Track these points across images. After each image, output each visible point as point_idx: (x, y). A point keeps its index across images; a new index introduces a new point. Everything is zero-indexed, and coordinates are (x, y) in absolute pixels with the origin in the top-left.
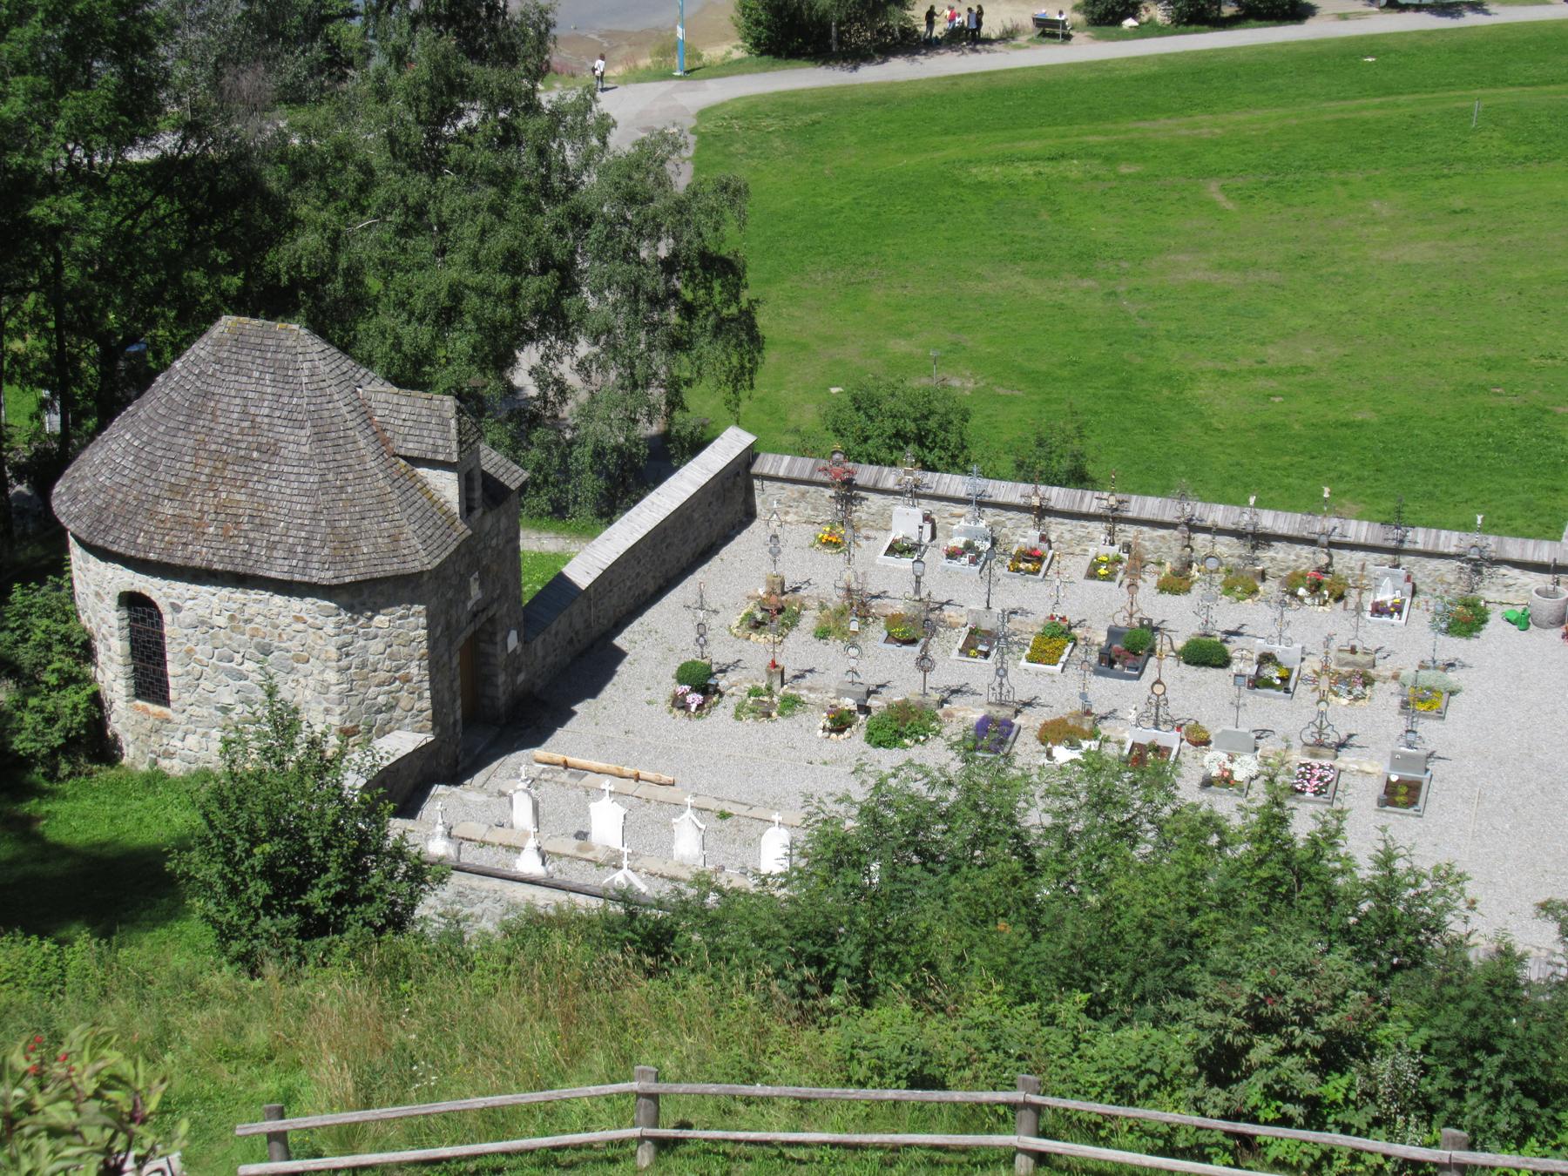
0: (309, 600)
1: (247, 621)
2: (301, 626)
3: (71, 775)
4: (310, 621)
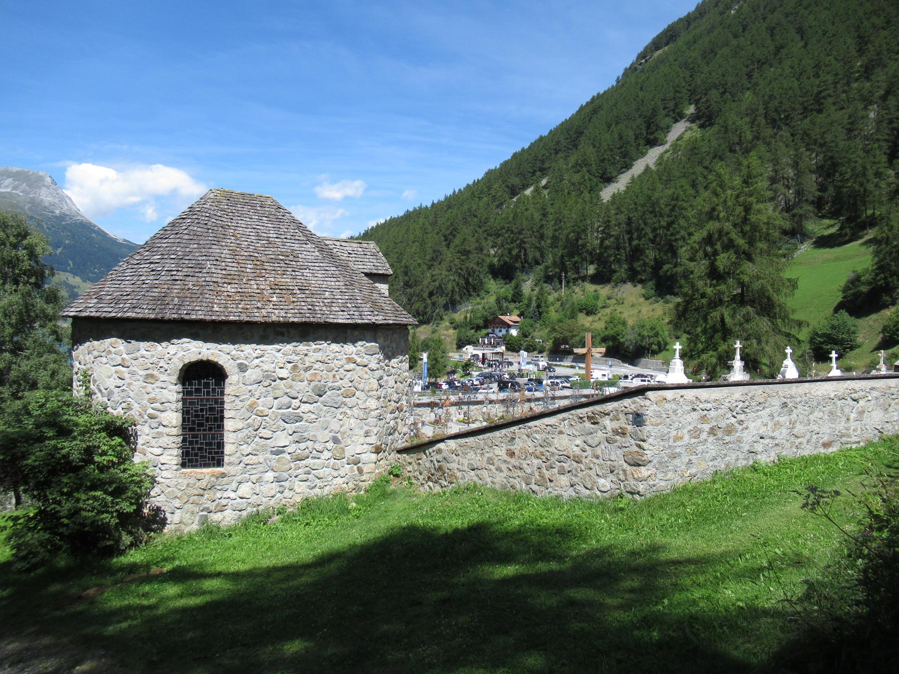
0: (360, 343)
1: (307, 369)
2: (352, 366)
3: (132, 545)
4: (359, 360)
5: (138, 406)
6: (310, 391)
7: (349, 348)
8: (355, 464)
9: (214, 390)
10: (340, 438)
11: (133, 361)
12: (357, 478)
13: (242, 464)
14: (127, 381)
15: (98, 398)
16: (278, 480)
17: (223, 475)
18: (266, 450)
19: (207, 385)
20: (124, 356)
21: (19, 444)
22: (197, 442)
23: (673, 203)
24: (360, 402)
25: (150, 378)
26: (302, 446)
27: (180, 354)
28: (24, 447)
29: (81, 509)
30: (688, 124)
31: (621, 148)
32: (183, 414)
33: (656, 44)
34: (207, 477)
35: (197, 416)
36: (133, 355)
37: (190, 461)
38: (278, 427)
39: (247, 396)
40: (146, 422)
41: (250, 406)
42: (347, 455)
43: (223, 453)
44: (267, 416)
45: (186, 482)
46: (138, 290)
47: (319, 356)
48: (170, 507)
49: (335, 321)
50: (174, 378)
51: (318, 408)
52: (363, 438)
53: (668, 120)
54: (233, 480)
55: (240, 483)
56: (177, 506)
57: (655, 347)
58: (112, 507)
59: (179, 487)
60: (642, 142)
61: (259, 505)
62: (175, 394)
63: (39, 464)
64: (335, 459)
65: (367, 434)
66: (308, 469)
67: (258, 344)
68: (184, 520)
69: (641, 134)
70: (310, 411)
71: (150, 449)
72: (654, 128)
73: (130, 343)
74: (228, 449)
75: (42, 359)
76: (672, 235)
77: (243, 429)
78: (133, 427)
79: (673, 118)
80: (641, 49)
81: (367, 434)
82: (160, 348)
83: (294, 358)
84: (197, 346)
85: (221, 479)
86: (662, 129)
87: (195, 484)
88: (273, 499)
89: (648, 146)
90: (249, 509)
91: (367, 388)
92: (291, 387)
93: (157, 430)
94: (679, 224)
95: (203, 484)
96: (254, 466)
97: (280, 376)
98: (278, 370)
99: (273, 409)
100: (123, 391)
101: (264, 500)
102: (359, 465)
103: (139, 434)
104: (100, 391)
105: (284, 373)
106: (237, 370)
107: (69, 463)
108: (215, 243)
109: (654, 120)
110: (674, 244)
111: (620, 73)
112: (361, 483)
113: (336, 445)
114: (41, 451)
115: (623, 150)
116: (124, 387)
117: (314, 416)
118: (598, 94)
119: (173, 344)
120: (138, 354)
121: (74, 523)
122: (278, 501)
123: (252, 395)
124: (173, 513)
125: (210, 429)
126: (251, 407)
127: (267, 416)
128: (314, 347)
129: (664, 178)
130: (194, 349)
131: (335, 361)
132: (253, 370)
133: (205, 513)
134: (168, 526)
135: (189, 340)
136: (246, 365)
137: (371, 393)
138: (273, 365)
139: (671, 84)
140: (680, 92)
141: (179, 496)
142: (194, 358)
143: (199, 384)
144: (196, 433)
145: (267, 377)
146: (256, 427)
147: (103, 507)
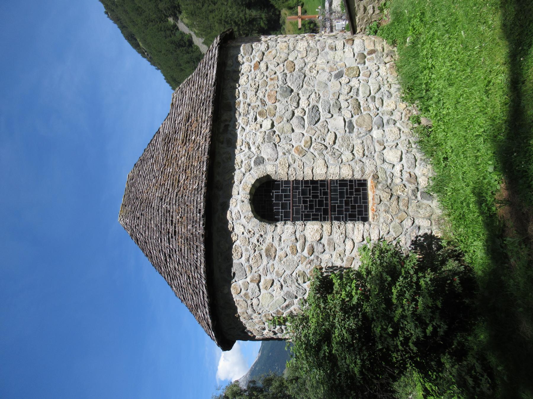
0: (240, 59)
1: (264, 103)
2: (263, 65)
4: (257, 59)
5: (300, 265)
6: (286, 100)
7: (244, 68)
8: (365, 57)
9: (283, 191)
10: (337, 71)
11: (254, 271)
12: (380, 55)
13: (364, 160)
14: (274, 276)
15: (295, 308)
16: (381, 125)
17: (376, 177)
18: (349, 138)
19: (278, 198)
20: (248, 280)
21: (337, 382)
22: (338, 207)
23: (223, 23)
24: (300, 56)
25: (270, 253)
26: (344, 105)
27: (243, 221)
28: (339, 376)
29: (414, 313)
30: (179, 21)
31: (194, 62)
32: (310, 220)
33: (136, 46)
34: (378, 192)
35: (311, 207)
36: (247, 270)
37: (360, 213)
38: (324, 127)
39: (290, 157)
40: (318, 257)
41: (300, 152)
42: (354, 65)
43: (351, 181)
44: (311, 137)
45: (383, 214)
46: (184, 268)
47: (250, 94)
48: (413, 230)
49: (214, 77)
50: (269, 228)
51: (304, 93)
52: (337, 51)
53: (177, 34)
54: (381, 168)
55: (384, 161)
56: (410, 222)
57: (312, 26)
58: (412, 277)
59: (389, 221)
60: (190, 49)
61: (409, 143)
62: (286, 226)
63: (360, 359)
64: (359, 75)
65: (334, 48)
66: (369, 99)
67: (235, 147)
68: (427, 215)
69: (185, 50)
70: (308, 99)
71: (347, 253)
72: (182, 42)
73: (234, 274)
74: (346, 174)
75: (309, 389)
76: (242, 22)
77: (324, 159)
78: (324, 270)
79: (176, 31)
80: (139, 56)
81: (334, 48)
82: (239, 243)
83: (251, 116)
84: (235, 204)
85: (380, 179)
86: (183, 37)
87: (386, 205)
88: (402, 129)
89: (193, 45)
90: (414, 151)
91: (286, 51)
92: (281, 117)
93: (326, 245)
94: (236, 18)
95: (385, 196)
96: (366, 148)
97: (270, 127)
98: (263, 129)
99: (304, 132)
100: (285, 282)
101: (403, 138)
102: (366, 53)
103: (330, 265)
104: (287, 307)
105: (267, 124)
106: (261, 166)
107: (359, 329)
108: (150, 205)
109: (177, 43)
110: (248, 20)
111: (154, 68)
112: (386, 51)
113: (344, 75)
114: (346, 358)
115: (195, 61)
116: (282, 281)
117: (313, 96)
118: (165, 79)
119: (233, 229)
120: (246, 265)
121: (432, 319)
122: (405, 125)
123: (289, 151)
124: (419, 228)
125: (325, 193)
126: (302, 152)
127: (311, 137)
128: (241, 98)
129: (209, 31)
130: (238, 207)
131: (257, 80)
132: (262, 152)
133: (419, 195)
134: (434, 233)
135: (228, 212)
136: (256, 158)
137: (291, 48)
138: (258, 133)
139: (156, 33)
140: (161, 28)
141: (399, 221)
142: (248, 207)
143: (278, 205)
144: (329, 207)
145: (270, 138)
146: (323, 147)
147: (412, 286)
